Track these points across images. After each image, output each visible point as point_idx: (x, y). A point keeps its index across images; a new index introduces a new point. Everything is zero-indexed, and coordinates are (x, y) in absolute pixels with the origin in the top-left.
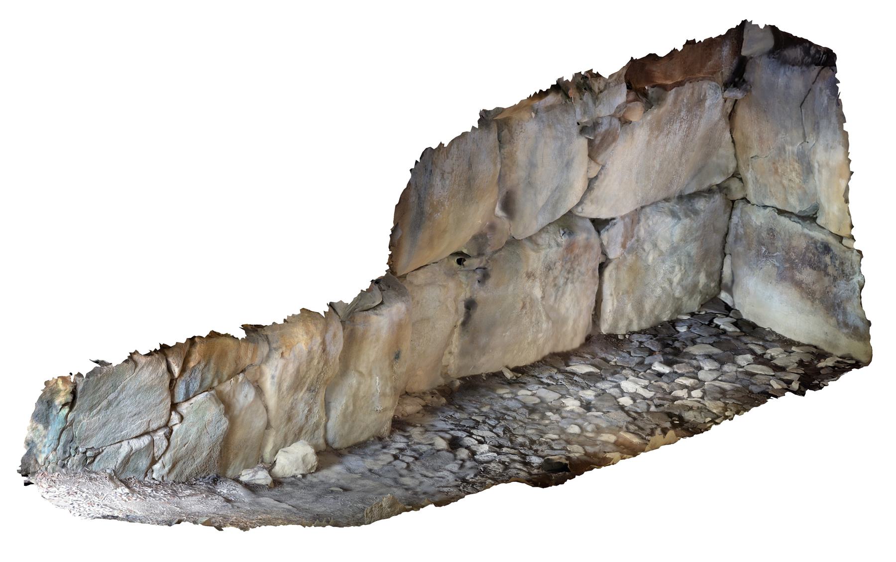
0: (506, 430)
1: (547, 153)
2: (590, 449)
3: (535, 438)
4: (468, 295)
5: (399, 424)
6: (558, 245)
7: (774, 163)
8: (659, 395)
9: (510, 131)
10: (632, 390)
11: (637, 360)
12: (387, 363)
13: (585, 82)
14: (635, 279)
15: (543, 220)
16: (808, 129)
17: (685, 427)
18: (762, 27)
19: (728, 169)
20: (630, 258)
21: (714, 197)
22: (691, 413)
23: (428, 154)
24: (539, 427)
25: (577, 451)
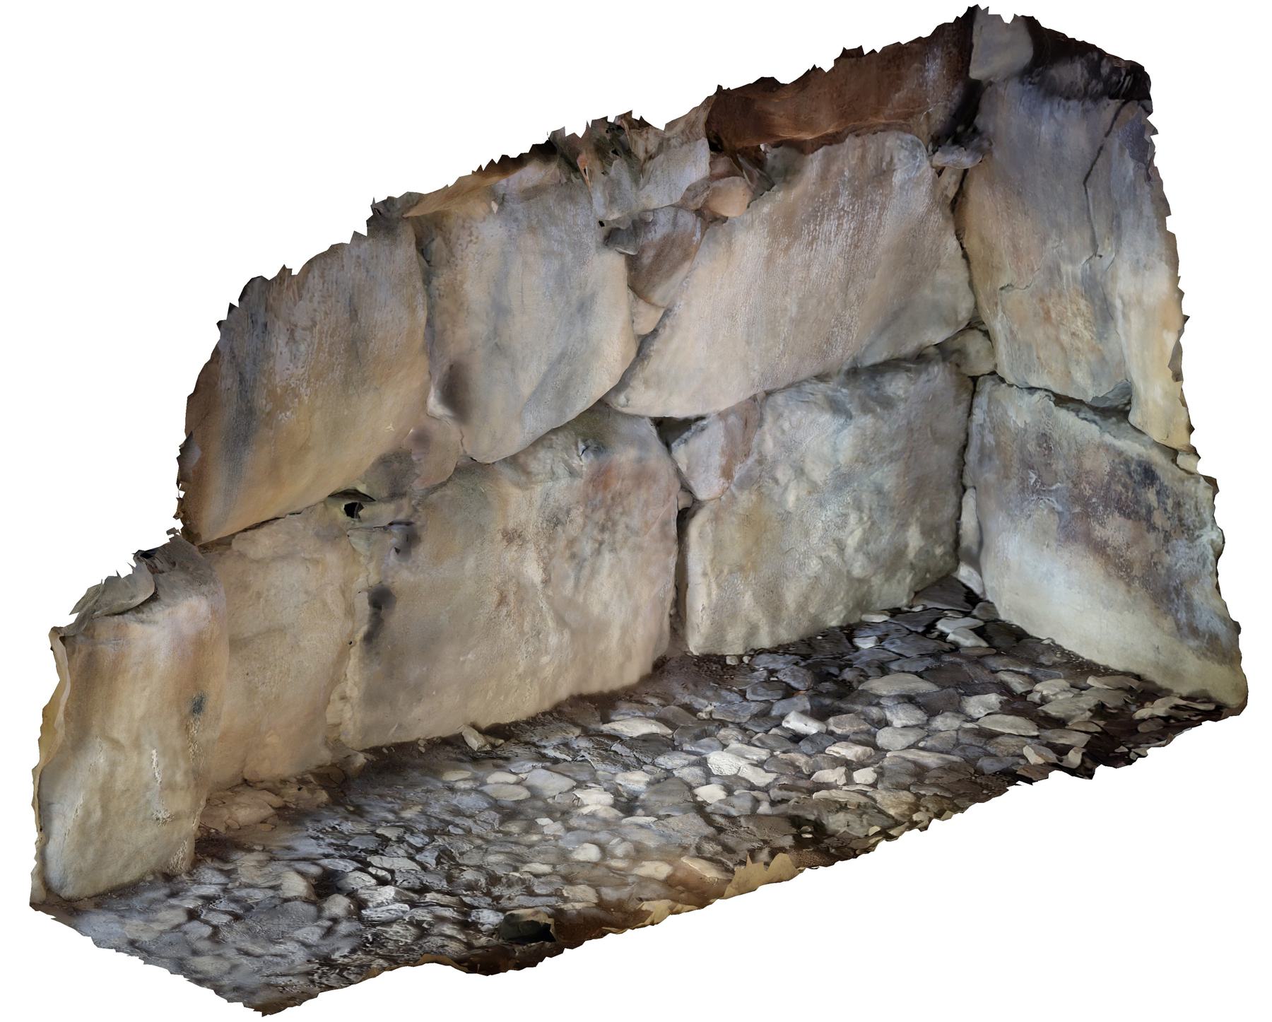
0: (444, 855)
1: (531, 286)
2: (610, 894)
3: (500, 872)
4: (374, 579)
5: (213, 847)
6: (572, 473)
7: (1042, 300)
8: (784, 781)
9: (447, 241)
10: (728, 771)
11: (755, 708)
12: (174, 722)
13: (615, 138)
14: (757, 542)
15: (536, 423)
16: (1101, 229)
17: (821, 844)
18: (1008, 19)
19: (956, 313)
20: (745, 499)
21: (929, 377)
22: (841, 816)
23: (256, 289)
24: (516, 849)
25: (580, 898)
